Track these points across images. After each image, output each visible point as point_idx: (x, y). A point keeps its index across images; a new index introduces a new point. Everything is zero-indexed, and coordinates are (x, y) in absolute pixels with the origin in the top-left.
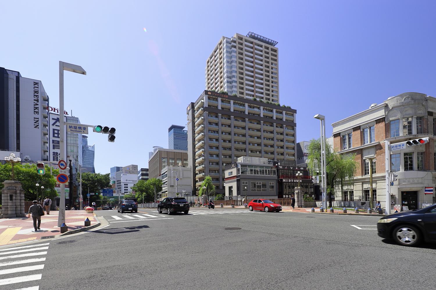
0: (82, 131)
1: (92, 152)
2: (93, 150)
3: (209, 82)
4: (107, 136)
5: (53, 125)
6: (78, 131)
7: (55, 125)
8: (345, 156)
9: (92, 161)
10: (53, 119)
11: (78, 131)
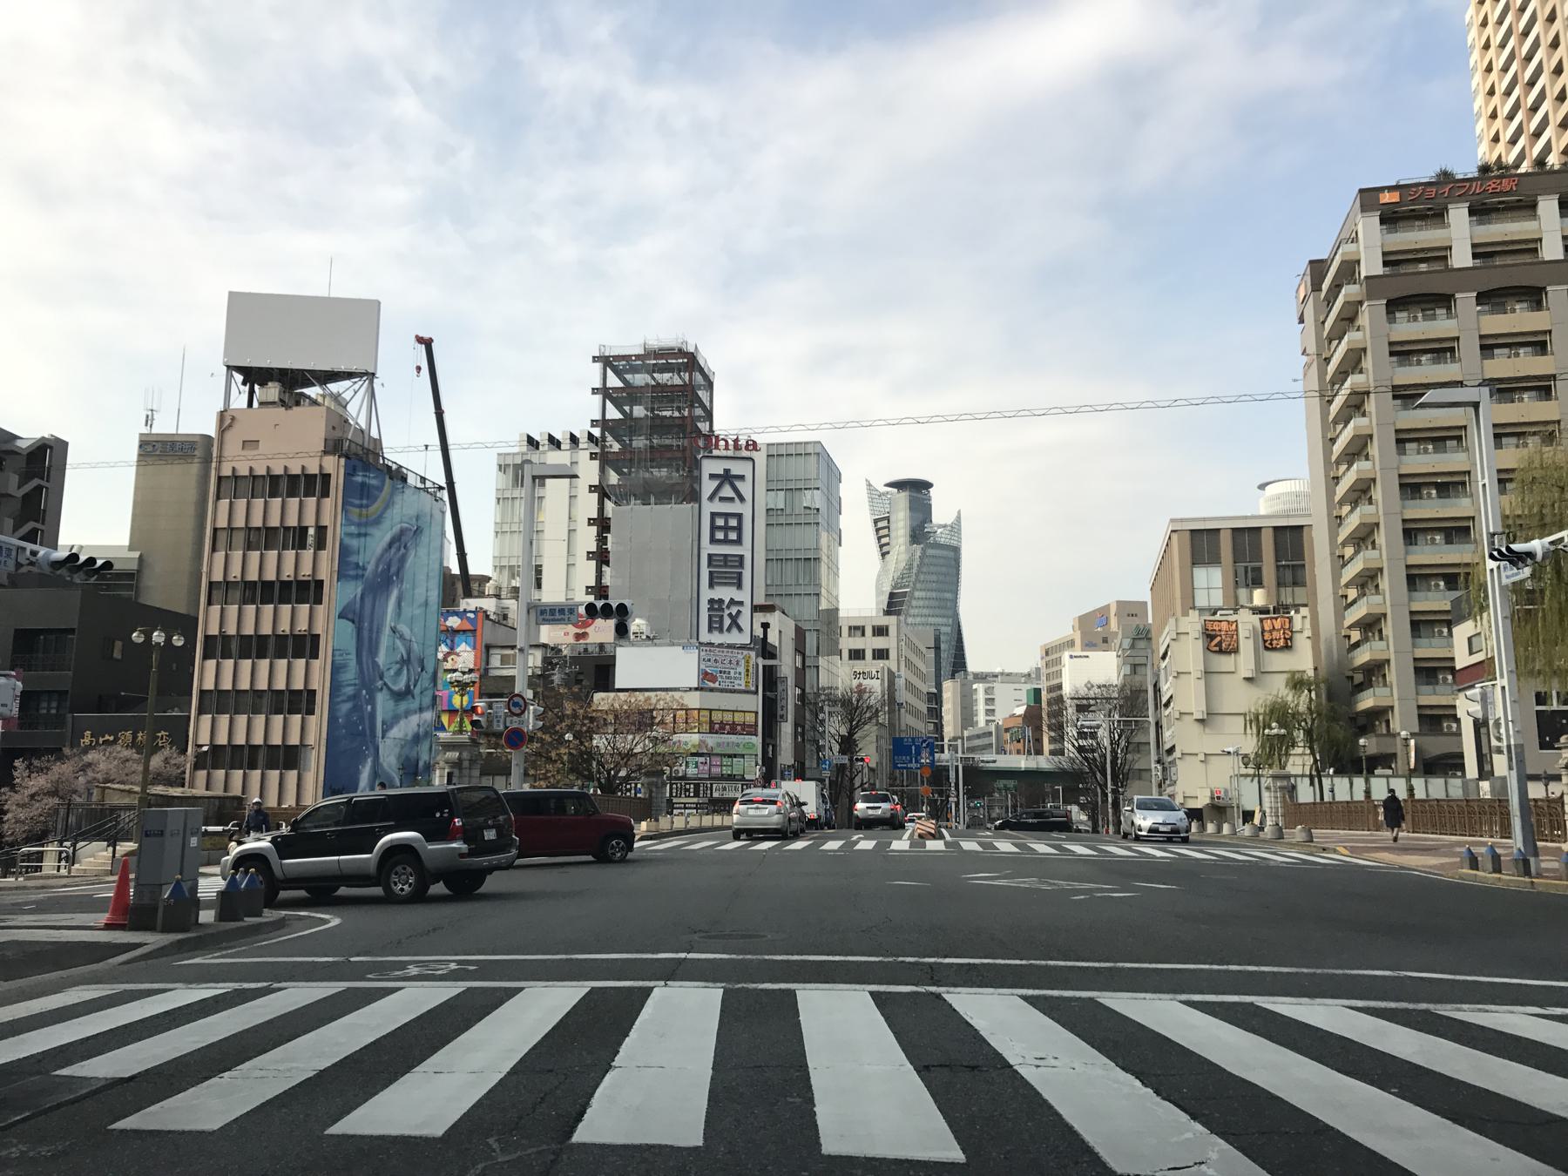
0: (566, 617)
1: (951, 554)
2: (954, 543)
3: (1495, 109)
4: (1307, 352)
5: (711, 498)
6: (558, 620)
7: (717, 499)
8: (1213, 758)
9: (948, 595)
10: (712, 476)
11: (558, 620)
